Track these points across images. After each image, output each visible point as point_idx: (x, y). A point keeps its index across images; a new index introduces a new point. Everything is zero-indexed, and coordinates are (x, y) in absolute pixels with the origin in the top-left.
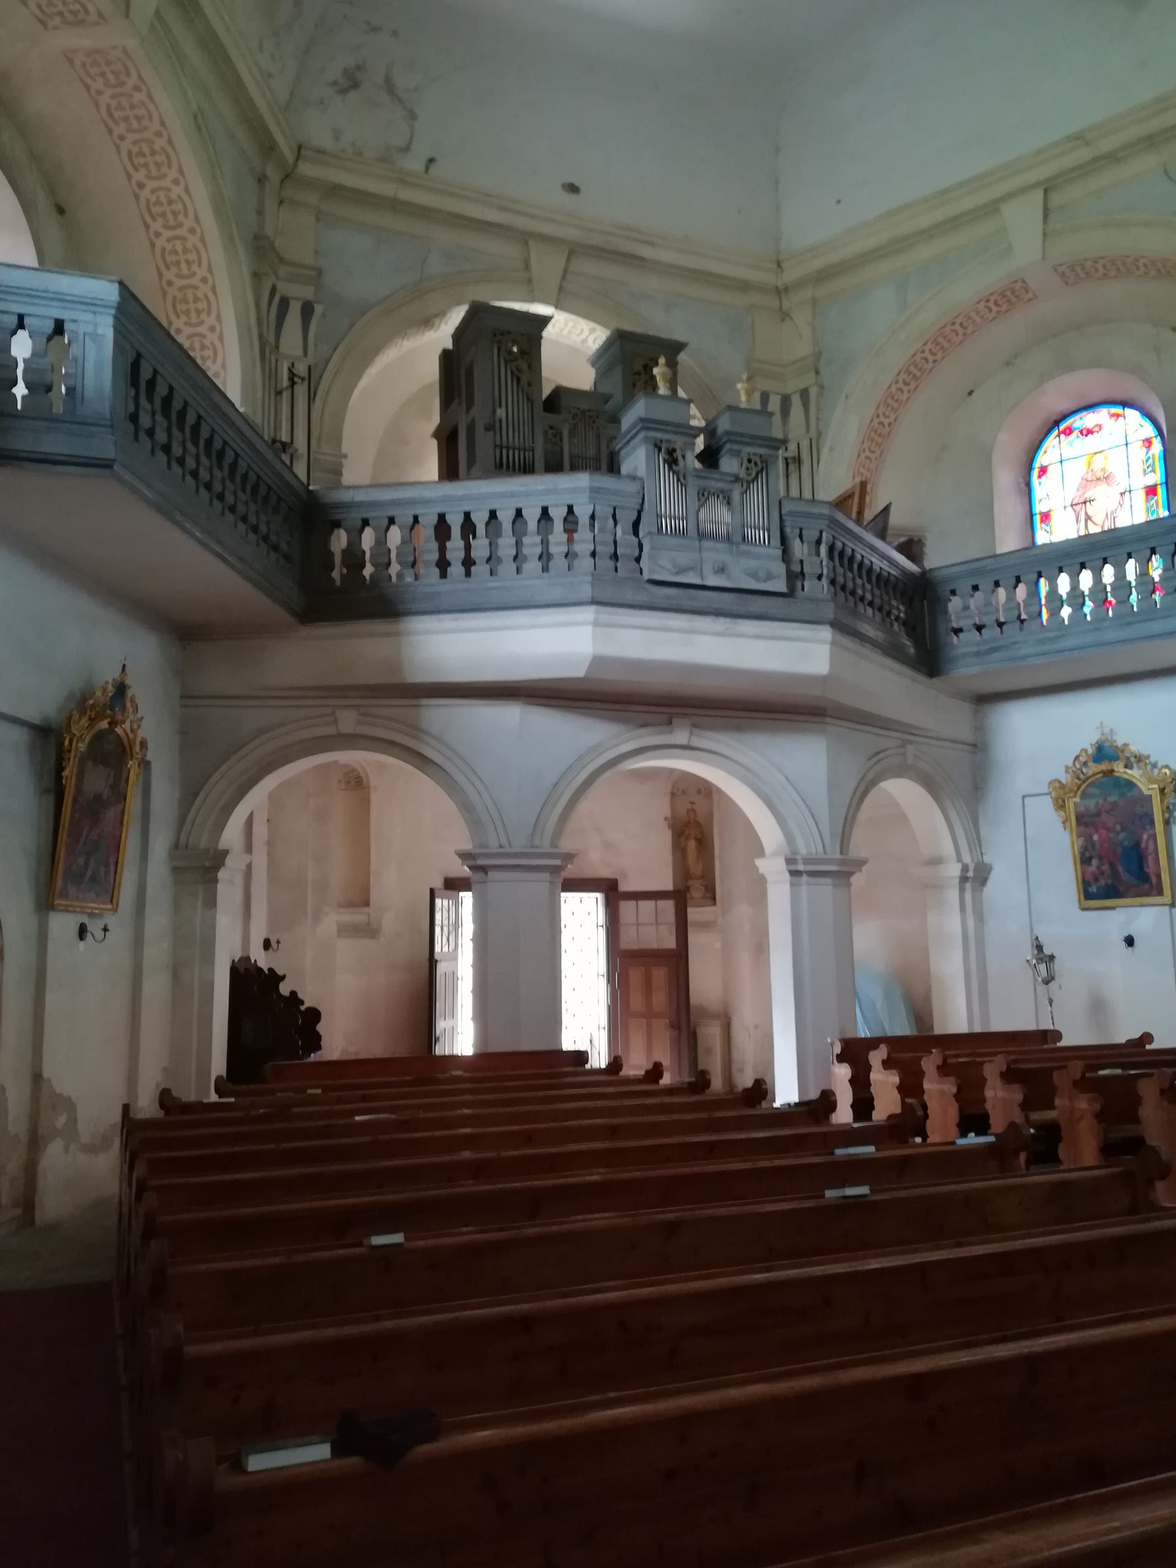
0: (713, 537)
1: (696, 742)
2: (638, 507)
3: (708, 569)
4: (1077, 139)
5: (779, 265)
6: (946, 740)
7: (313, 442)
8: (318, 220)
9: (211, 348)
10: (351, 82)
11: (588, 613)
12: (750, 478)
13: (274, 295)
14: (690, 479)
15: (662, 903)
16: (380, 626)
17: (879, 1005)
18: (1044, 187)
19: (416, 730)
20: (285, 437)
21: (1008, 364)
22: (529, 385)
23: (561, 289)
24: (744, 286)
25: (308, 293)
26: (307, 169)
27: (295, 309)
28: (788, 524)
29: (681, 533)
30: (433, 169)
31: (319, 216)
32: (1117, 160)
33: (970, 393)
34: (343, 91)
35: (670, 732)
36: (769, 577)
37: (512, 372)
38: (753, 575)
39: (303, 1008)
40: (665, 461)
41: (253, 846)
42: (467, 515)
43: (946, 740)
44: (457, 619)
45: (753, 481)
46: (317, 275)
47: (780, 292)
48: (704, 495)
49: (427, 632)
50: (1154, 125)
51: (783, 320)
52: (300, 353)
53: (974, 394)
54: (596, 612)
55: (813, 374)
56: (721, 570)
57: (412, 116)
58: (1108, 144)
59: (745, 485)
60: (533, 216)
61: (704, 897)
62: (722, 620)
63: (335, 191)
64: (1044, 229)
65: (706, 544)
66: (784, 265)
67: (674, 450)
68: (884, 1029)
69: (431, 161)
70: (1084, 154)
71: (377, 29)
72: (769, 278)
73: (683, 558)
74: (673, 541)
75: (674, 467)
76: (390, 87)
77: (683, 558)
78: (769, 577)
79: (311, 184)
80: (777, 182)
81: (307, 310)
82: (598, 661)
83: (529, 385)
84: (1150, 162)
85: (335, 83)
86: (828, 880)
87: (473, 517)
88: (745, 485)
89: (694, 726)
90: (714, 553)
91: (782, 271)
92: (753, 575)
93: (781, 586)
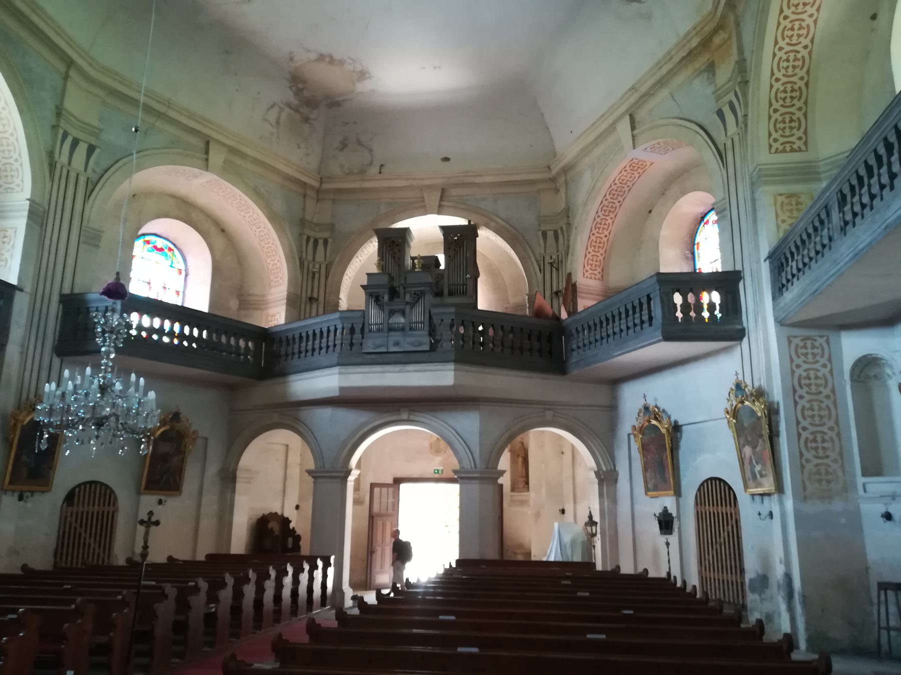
0: (395, 330)
1: (412, 418)
2: (362, 322)
3: (391, 343)
4: (633, 89)
5: (549, 168)
6: (572, 406)
7: (327, 296)
8: (334, 203)
9: (783, 116)
10: (344, 145)
11: (336, 370)
12: (414, 302)
13: (739, 98)
14: (385, 307)
15: (382, 490)
16: (281, 380)
17: (568, 546)
18: (629, 113)
19: (297, 419)
20: (315, 296)
21: (663, 194)
22: (399, 259)
23: (440, 206)
24: (532, 182)
25: (326, 235)
26: (326, 186)
27: (321, 242)
28: (434, 318)
29: (379, 330)
30: (384, 170)
31: (334, 201)
32: (653, 94)
33: (650, 212)
34: (341, 150)
35: (400, 414)
36: (420, 344)
37: (391, 255)
38: (412, 344)
39: (296, 534)
40: (375, 301)
41: (736, 450)
42: (314, 330)
43: (572, 406)
44: (301, 375)
45: (416, 302)
46: (331, 227)
47: (553, 180)
48: (392, 313)
49: (294, 381)
50: (658, 76)
51: (557, 193)
52: (323, 260)
53: (652, 212)
54: (339, 369)
55: (566, 218)
56: (397, 344)
57: (371, 150)
58: (643, 89)
59: (412, 305)
60: (422, 179)
61: (524, 487)
62: (399, 365)
63: (339, 191)
64: (632, 134)
65: (392, 333)
66: (551, 167)
67: (379, 296)
68: (569, 559)
69: (382, 165)
70: (636, 96)
71: (347, 124)
72: (546, 176)
73: (379, 341)
74: (377, 334)
75: (379, 303)
76: (359, 143)
77: (379, 341)
78: (420, 344)
79: (327, 191)
80: (548, 128)
81: (326, 242)
82: (342, 389)
83: (399, 259)
84: (664, 93)
85: (337, 148)
86: (477, 481)
87: (323, 329)
88: (412, 305)
89: (410, 411)
90: (395, 336)
91: (551, 171)
92: (412, 344)
93: (427, 348)
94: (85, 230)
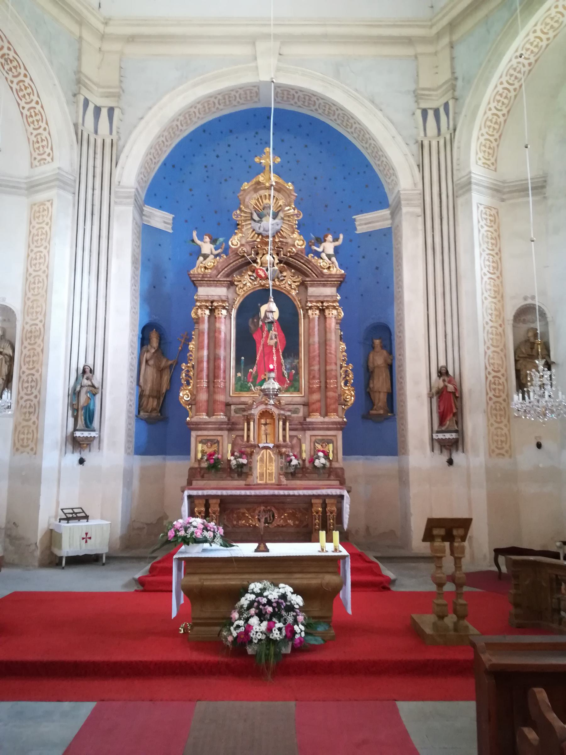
26: (109, 30)
94: (116, 192)
